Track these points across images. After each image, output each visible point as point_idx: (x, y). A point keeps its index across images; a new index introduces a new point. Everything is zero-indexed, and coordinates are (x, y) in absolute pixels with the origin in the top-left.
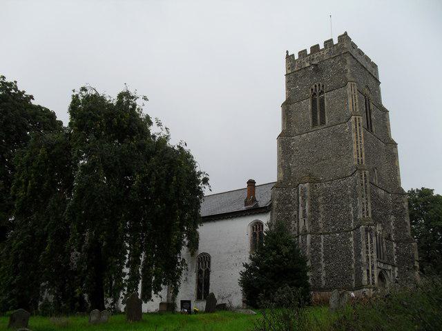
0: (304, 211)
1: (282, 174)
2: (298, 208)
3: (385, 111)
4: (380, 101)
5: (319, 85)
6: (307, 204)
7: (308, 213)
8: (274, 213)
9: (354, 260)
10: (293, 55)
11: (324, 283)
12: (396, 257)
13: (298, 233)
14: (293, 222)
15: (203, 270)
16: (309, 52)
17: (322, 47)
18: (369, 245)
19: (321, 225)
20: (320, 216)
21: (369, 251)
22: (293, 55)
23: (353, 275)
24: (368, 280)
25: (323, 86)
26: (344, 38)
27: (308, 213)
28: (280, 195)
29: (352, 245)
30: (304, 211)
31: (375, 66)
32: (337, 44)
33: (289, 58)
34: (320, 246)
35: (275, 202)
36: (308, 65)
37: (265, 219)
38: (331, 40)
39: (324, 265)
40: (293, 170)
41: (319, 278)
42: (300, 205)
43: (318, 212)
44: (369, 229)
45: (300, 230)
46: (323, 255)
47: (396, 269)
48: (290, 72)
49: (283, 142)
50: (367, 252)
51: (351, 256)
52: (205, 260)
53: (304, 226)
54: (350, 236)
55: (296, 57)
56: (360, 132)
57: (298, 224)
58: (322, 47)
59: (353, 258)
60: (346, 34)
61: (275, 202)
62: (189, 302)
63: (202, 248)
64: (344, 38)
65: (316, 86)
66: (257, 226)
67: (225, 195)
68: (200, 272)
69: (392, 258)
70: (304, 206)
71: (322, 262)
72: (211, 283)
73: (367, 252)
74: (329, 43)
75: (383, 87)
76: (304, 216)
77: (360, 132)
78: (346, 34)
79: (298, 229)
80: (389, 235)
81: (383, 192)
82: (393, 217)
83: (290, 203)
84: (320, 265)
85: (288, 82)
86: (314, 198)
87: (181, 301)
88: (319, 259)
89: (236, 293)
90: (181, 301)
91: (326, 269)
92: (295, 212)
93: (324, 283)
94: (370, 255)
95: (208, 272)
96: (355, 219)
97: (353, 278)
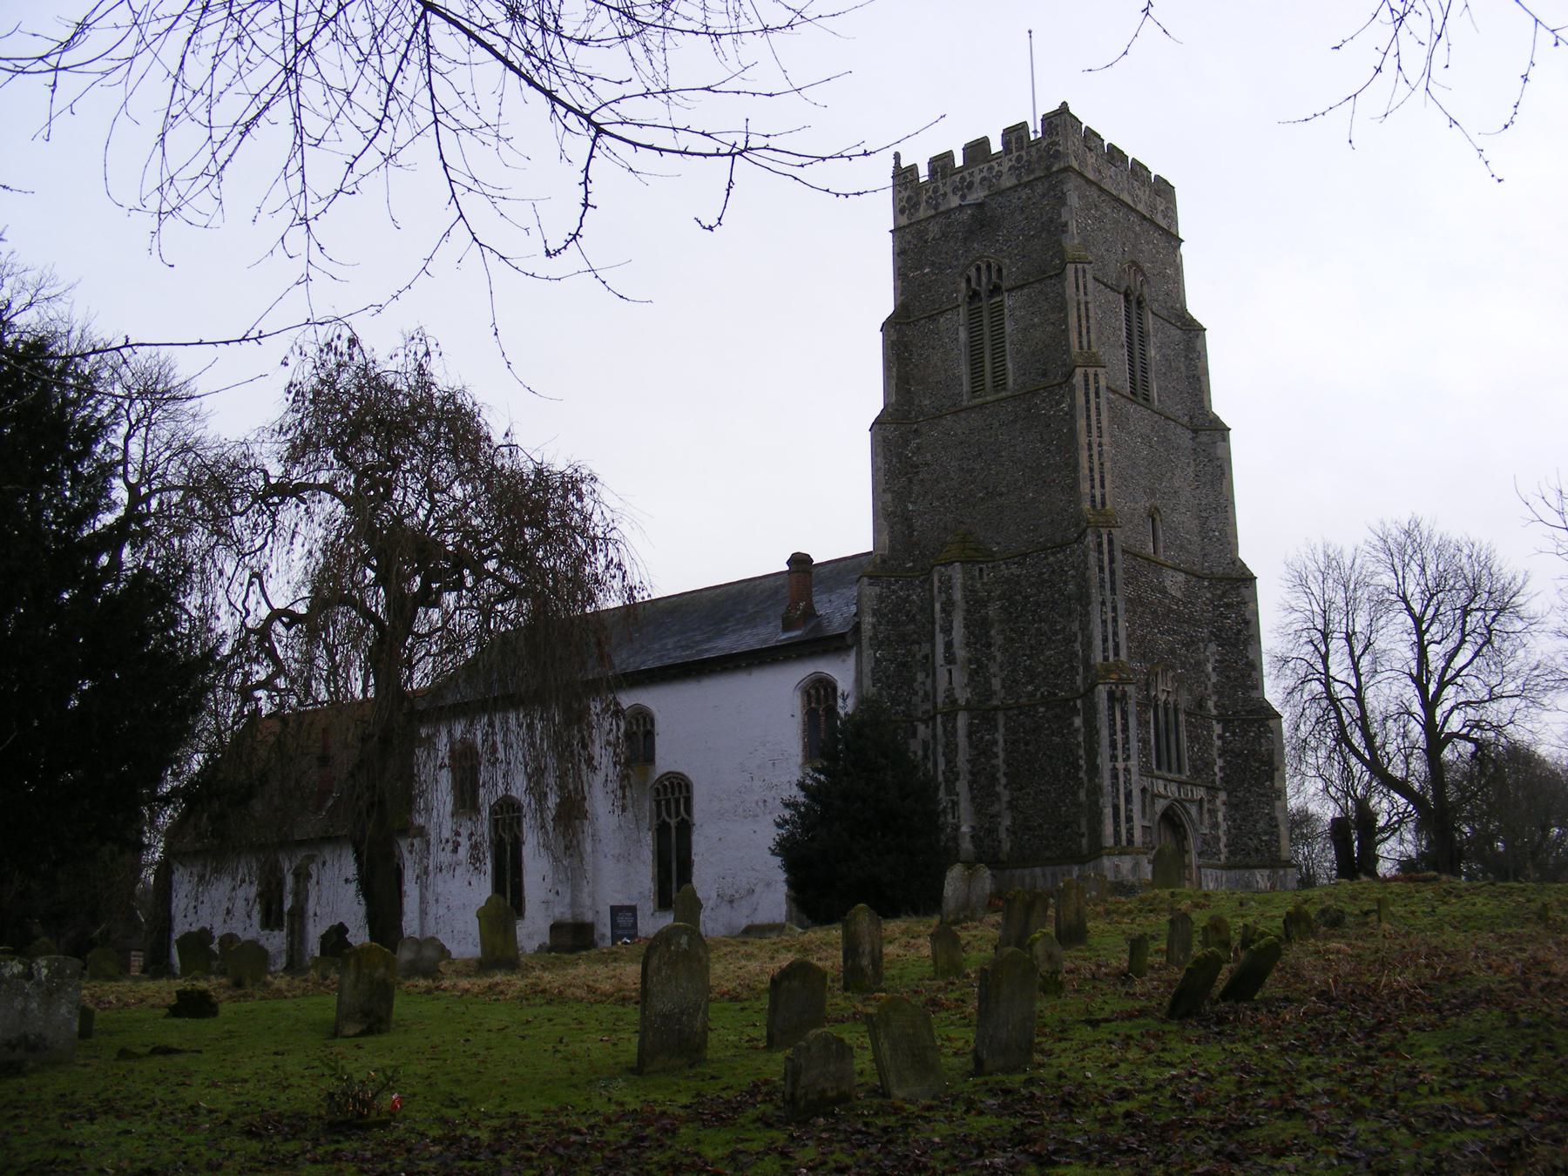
0: (949, 645)
1: (885, 538)
2: (933, 637)
3: (1193, 332)
4: (1184, 308)
5: (989, 266)
6: (955, 624)
7: (961, 653)
8: (868, 652)
9: (1085, 779)
10: (913, 169)
11: (1006, 846)
12: (1220, 762)
13: (935, 706)
14: (920, 677)
15: (673, 822)
16: (959, 162)
17: (996, 146)
18: (1119, 737)
19: (996, 684)
20: (994, 658)
21: (1119, 752)
22: (913, 169)
23: (1084, 822)
24: (1117, 833)
25: (1000, 270)
26: (1060, 120)
27: (961, 653)
28: (881, 599)
29: (1081, 739)
30: (949, 645)
31: (1164, 190)
32: (1038, 141)
33: (903, 176)
34: (995, 742)
35: (868, 620)
36: (955, 201)
37: (842, 673)
38: (1023, 126)
39: (1006, 796)
40: (917, 522)
41: (992, 831)
42: (937, 628)
43: (989, 645)
44: (1118, 694)
45: (940, 700)
46: (1003, 767)
47: (1222, 796)
48: (904, 221)
49: (885, 439)
50: (1114, 758)
51: (1078, 768)
52: (676, 792)
53: (950, 691)
54: (1075, 711)
55: (924, 173)
56: (1099, 414)
57: (934, 682)
58: (996, 146)
59: (1082, 775)
60: (1064, 104)
61: (868, 620)
62: (632, 910)
63: (667, 759)
64: (1060, 120)
65: (978, 269)
66: (819, 694)
67: (771, 579)
68: (662, 831)
69: (1209, 765)
70: (947, 630)
71: (999, 789)
72: (696, 858)
73: (1114, 758)
74: (1015, 134)
75: (1189, 254)
76: (950, 659)
77: (1099, 414)
78: (1064, 104)
79: (935, 697)
80: (1201, 704)
81: (1181, 577)
82: (1213, 647)
83: (912, 619)
84: (997, 796)
85: (900, 254)
86: (975, 603)
87: (613, 908)
88: (994, 779)
89: (768, 885)
90: (613, 908)
91: (1012, 805)
92: (926, 648)
93: (1006, 846)
94: (1120, 765)
95: (685, 828)
96: (1088, 666)
97: (1084, 829)
